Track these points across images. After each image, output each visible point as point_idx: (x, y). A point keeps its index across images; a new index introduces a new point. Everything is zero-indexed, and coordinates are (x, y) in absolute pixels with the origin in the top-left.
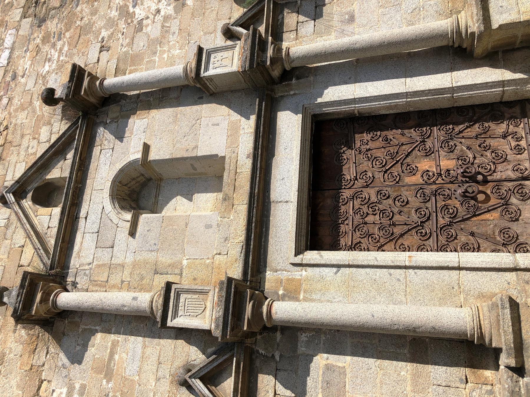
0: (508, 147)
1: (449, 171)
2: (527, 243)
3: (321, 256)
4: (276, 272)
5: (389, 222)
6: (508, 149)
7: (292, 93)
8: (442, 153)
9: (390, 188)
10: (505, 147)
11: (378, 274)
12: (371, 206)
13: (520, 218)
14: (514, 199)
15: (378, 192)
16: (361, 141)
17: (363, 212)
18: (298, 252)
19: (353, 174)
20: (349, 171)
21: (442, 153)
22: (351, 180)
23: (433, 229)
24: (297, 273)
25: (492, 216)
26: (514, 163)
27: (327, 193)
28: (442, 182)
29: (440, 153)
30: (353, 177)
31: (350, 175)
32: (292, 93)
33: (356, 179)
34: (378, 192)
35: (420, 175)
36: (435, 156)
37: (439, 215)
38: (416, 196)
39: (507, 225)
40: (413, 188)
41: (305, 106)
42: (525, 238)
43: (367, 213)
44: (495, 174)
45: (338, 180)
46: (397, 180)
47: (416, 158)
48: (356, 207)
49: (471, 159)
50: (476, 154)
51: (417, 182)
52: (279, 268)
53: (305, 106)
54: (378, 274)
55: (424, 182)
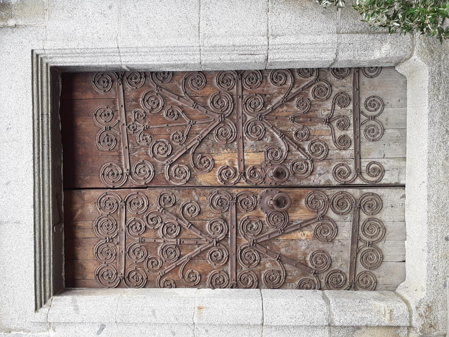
0: (331, 138)
1: (255, 168)
2: (341, 272)
3: (76, 309)
4: (10, 332)
5: (175, 240)
6: (331, 141)
7: (11, 22)
8: (249, 142)
9: (177, 191)
10: (327, 138)
11: (157, 334)
12: (151, 216)
13: (337, 238)
14: (333, 213)
15: (161, 196)
16: (135, 112)
17: (141, 226)
18: (40, 302)
19: (126, 167)
20: (120, 161)
21: (249, 142)
22: (122, 174)
23: (232, 252)
24: (42, 333)
25: (304, 234)
26: (337, 163)
27: (90, 195)
28: (246, 184)
29: (245, 141)
30: (125, 171)
31: (121, 166)
32: (11, 22)
33: (130, 173)
34: (161, 196)
35: (217, 174)
36: (238, 144)
37: (240, 231)
38: (212, 204)
39: (321, 246)
40: (208, 191)
41: (36, 52)
42: (339, 264)
43: (146, 227)
44: (312, 178)
45: (103, 174)
46: (188, 178)
47: (213, 146)
48: (130, 219)
49: (284, 153)
50: (291, 146)
51: (213, 183)
52: (13, 326)
53: (36, 52)
54: (157, 334)
55: (222, 184)
